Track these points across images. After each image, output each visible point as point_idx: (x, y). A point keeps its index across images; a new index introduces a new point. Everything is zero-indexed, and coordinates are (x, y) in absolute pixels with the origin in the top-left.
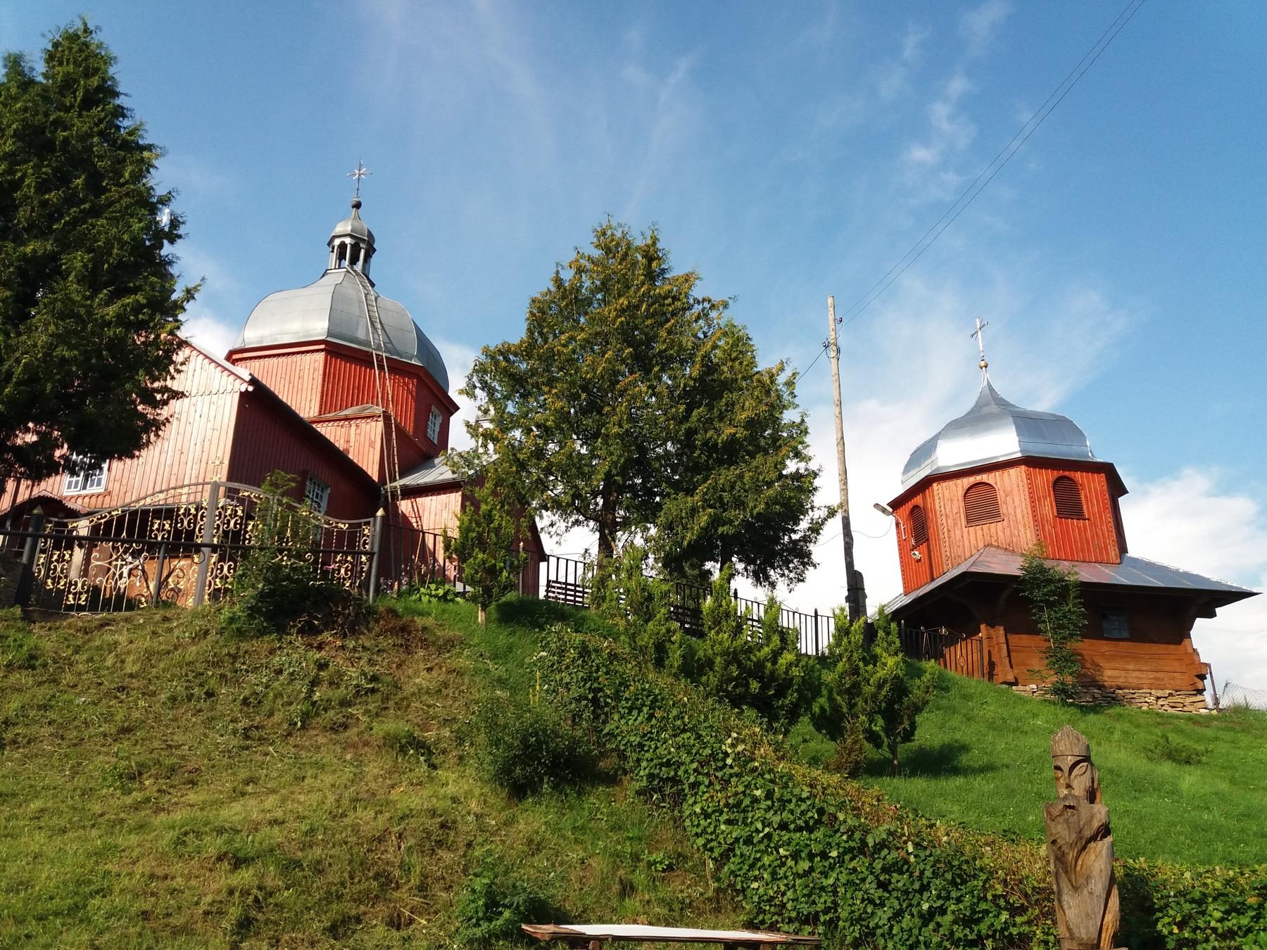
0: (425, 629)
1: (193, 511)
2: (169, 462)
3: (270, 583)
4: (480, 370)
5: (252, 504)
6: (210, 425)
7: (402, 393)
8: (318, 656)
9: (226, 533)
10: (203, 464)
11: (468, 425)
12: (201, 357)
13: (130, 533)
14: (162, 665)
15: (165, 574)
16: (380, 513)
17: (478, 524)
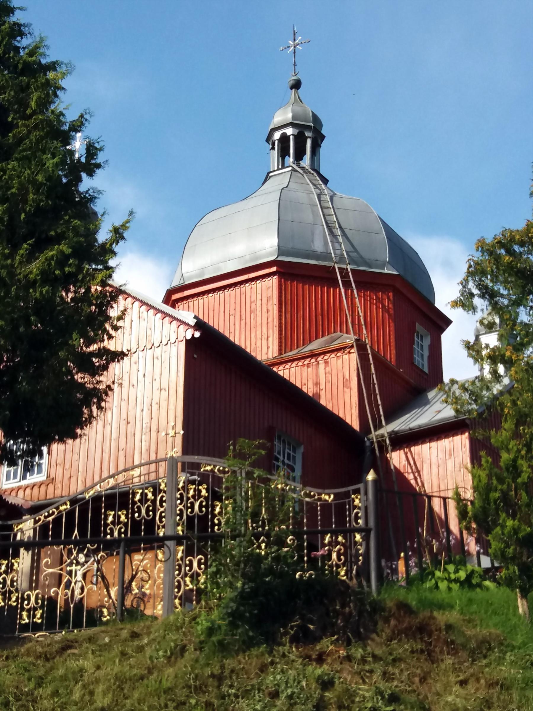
0: (449, 627)
1: (150, 496)
2: (114, 436)
3: (250, 580)
4: (476, 271)
5: (218, 481)
6: (156, 385)
7: (377, 314)
8: (319, 671)
9: (190, 519)
10: (154, 434)
11: (468, 346)
12: (137, 304)
13: (83, 532)
14: (136, 695)
15: (127, 577)
16: (371, 476)
17: (501, 480)
